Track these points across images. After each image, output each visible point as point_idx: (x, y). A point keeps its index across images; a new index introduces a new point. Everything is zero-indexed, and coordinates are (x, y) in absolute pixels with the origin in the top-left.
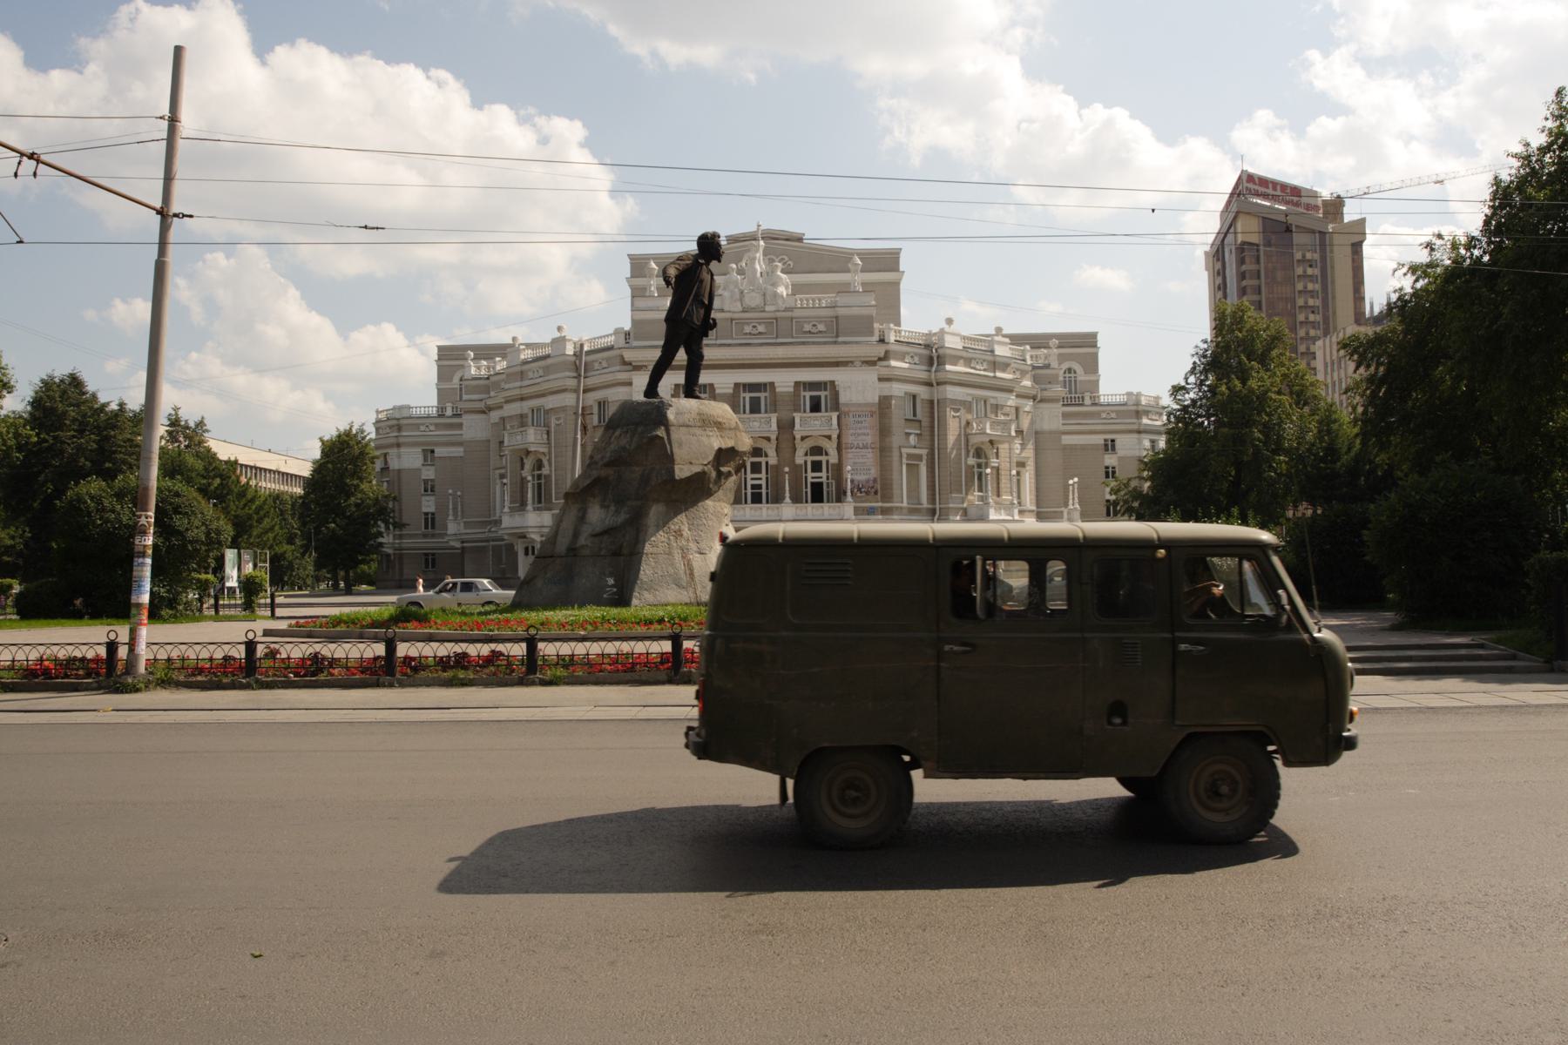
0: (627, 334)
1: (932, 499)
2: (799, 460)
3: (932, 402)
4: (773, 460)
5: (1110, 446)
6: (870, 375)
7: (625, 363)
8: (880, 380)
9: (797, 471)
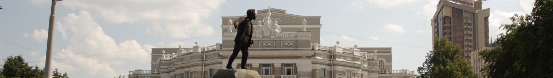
0: (221, 45)
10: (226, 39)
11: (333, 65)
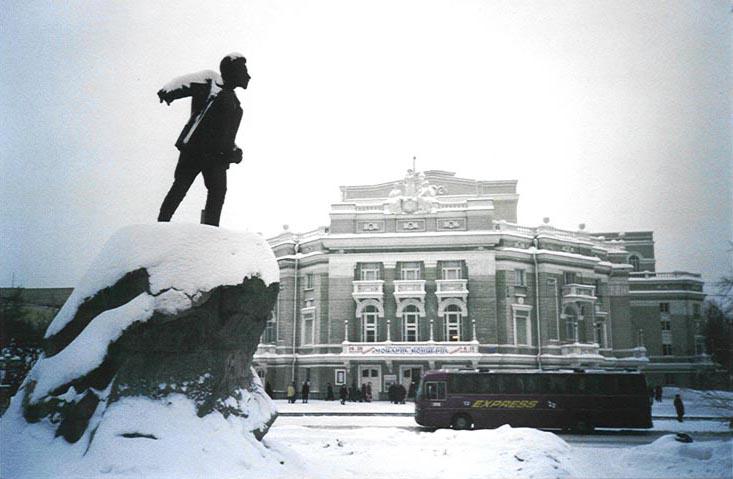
1: (535, 342)
2: (441, 314)
3: (534, 275)
4: (464, 313)
5: (665, 308)
6: (491, 256)
7: (325, 248)
8: (497, 259)
9: (439, 322)
10: (335, 217)
11: (539, 262)
